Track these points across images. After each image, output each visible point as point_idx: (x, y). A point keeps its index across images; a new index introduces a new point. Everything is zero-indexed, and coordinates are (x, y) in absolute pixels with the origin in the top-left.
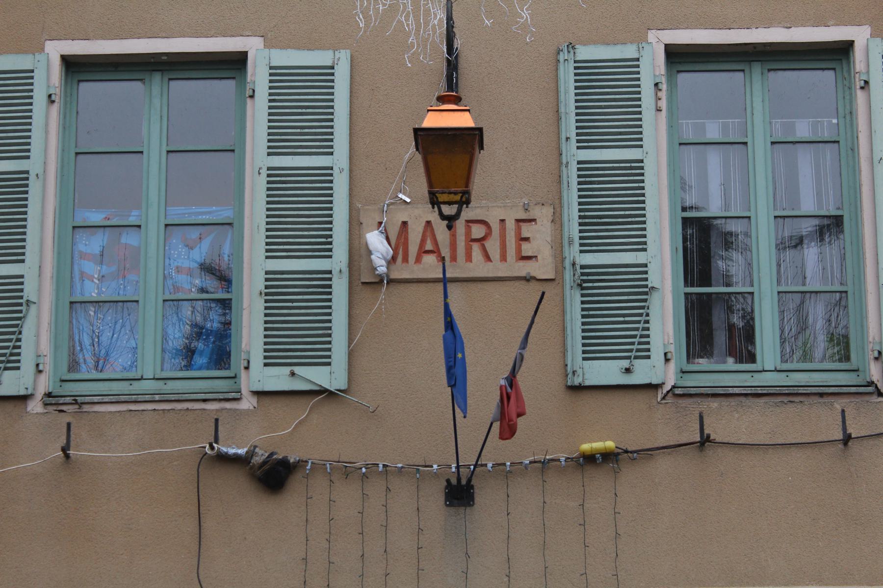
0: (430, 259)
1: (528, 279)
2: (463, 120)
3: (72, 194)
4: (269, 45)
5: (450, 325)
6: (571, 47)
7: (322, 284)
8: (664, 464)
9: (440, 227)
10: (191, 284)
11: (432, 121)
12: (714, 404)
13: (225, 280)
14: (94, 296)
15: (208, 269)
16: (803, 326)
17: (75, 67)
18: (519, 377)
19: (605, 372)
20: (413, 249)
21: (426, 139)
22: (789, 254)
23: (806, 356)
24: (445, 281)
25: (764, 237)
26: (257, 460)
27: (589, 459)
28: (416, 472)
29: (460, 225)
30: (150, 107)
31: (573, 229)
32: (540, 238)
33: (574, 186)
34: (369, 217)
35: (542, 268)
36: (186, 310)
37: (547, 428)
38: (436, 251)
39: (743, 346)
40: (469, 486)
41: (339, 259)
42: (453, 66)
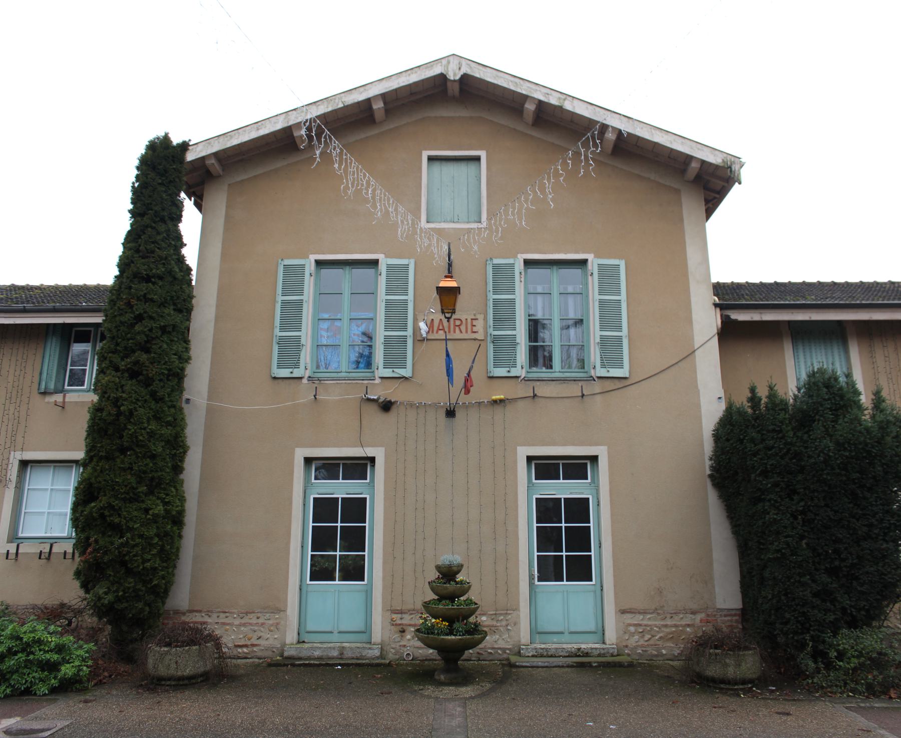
8: (521, 404)
34: (420, 317)
41: (410, 332)
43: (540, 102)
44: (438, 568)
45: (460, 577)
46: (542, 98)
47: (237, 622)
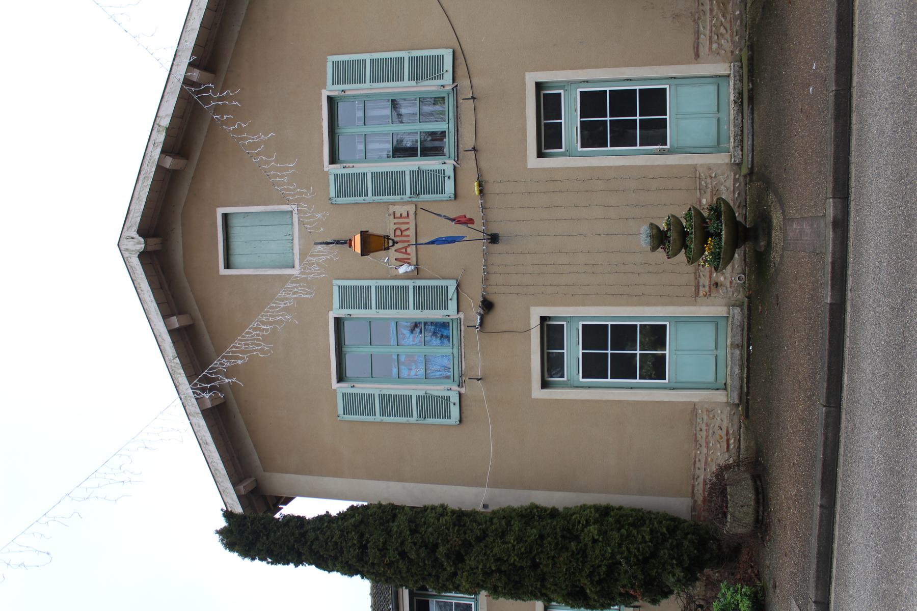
0: (409, 250)
1: (416, 214)
2: (358, 238)
3: (387, 379)
4: (331, 309)
5: (433, 242)
6: (330, 199)
7: (418, 289)
8: (483, 165)
9: (397, 246)
10: (418, 337)
11: (358, 249)
12: (461, 146)
13: (416, 325)
14: (423, 371)
15: (412, 331)
16: (431, 114)
17: (341, 378)
18: (452, 217)
19: (449, 186)
20: (405, 256)
21: (365, 251)
22: (404, 119)
23: (443, 113)
24: (417, 244)
25: (398, 128)
26: (482, 312)
27: (481, 191)
28: (486, 254)
29: (396, 239)
30: (356, 351)
31: (397, 198)
32: (400, 210)
33: (381, 197)
34: (394, 273)
35: (412, 209)
36: (428, 339)
37: (471, 207)
38: (406, 248)
39: (439, 136)
40: (491, 235)
41: (409, 283)
42: (338, 242)
43: (162, 152)
44: (654, 249)
45: (663, 226)
46: (159, 150)
47: (704, 450)
